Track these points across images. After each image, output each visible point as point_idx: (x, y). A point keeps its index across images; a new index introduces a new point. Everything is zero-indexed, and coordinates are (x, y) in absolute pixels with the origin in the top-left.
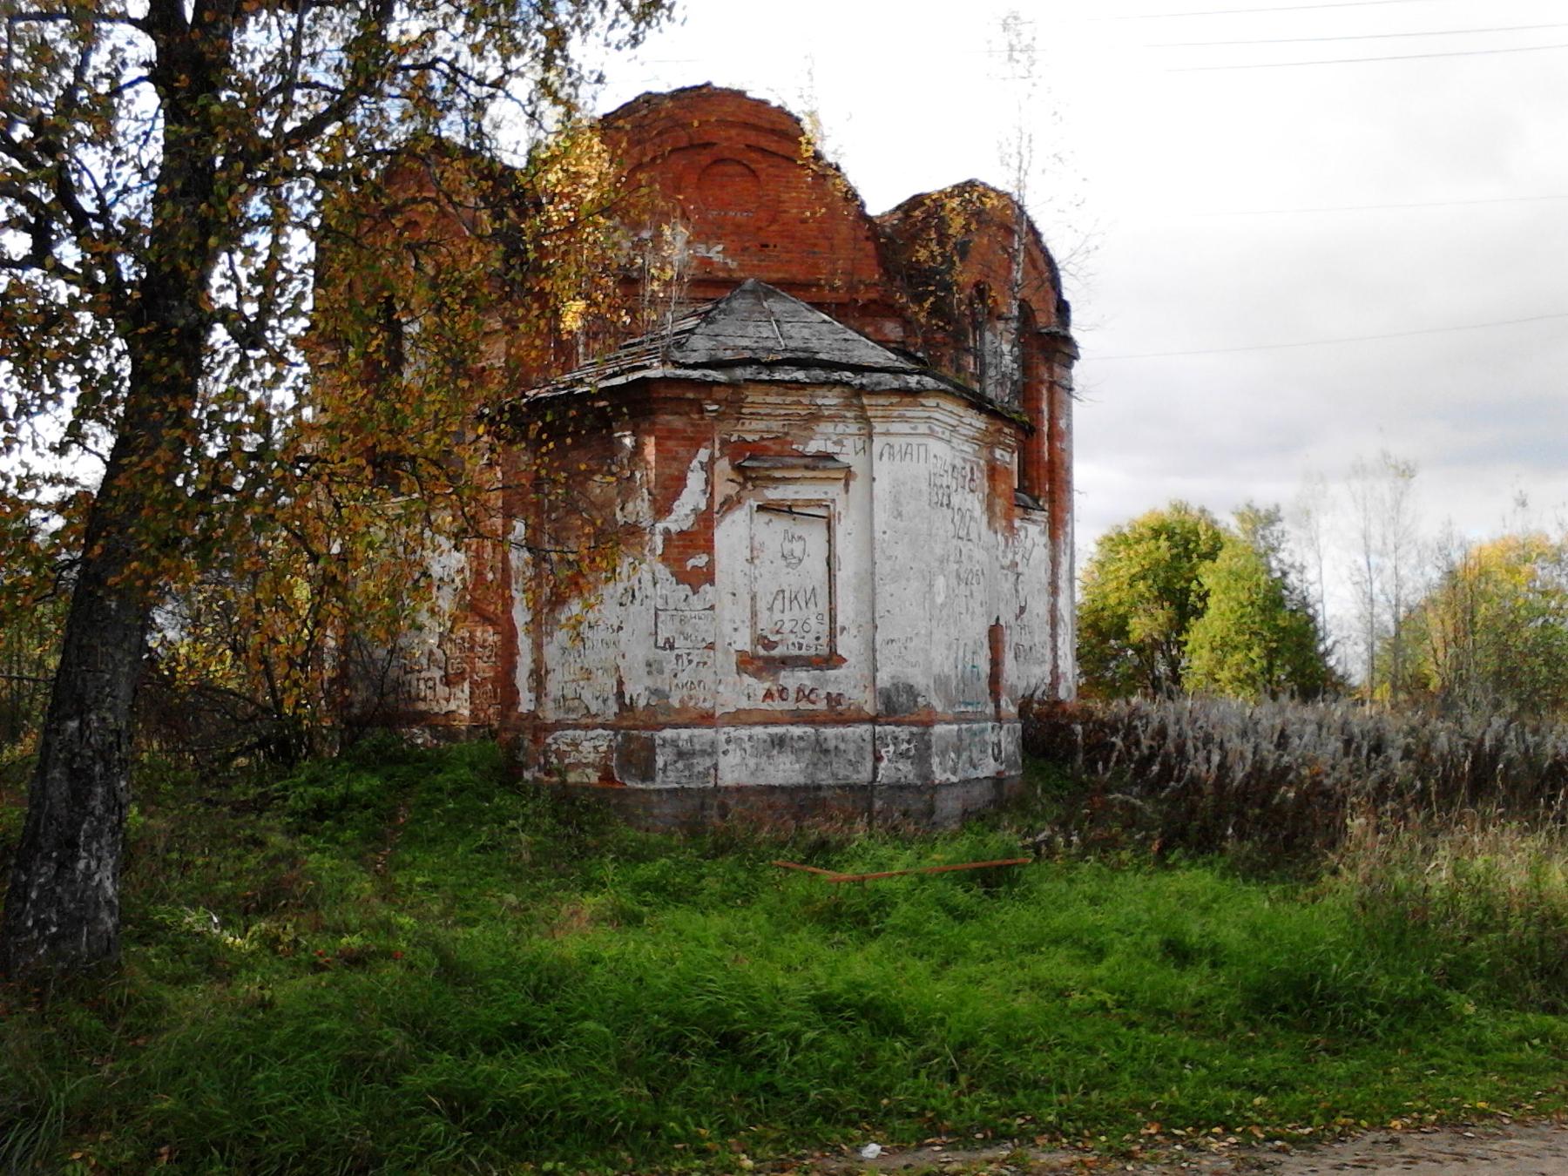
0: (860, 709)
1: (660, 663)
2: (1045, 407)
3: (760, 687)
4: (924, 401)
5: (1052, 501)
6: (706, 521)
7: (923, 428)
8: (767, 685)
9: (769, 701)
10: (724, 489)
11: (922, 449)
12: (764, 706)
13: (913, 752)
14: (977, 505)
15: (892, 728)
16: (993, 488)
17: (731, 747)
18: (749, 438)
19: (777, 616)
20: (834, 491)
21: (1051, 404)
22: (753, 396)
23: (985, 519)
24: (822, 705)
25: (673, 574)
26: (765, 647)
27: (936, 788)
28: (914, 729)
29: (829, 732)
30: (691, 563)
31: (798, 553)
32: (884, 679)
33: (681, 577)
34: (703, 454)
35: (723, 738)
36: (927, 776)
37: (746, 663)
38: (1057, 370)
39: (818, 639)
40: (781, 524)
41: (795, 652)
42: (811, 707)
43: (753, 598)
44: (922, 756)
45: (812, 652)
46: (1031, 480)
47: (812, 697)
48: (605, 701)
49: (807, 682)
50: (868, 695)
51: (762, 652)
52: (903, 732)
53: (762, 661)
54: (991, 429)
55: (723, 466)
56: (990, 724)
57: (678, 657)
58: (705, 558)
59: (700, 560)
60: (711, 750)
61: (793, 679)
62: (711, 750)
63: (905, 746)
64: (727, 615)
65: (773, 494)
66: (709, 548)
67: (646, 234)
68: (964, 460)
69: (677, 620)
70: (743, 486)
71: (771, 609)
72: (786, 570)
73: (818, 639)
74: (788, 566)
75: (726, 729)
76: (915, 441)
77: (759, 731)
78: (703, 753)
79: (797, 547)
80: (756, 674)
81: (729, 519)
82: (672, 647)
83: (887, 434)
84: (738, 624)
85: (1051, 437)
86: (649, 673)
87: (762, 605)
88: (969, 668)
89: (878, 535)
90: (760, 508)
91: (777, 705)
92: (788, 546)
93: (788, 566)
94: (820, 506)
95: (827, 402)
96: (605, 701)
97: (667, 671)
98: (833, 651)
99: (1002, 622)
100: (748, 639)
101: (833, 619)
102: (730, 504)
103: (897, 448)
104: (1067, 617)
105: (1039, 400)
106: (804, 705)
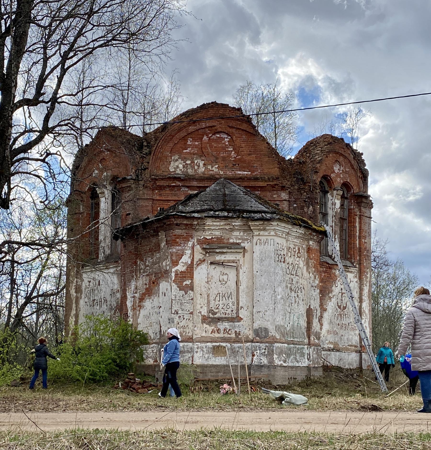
0: (248, 337)
1: (173, 319)
2: (357, 225)
3: (210, 328)
4: (272, 223)
5: (360, 264)
6: (191, 268)
7: (273, 233)
8: (213, 328)
9: (213, 334)
10: (198, 256)
11: (272, 240)
12: (211, 335)
13: (266, 353)
14: (301, 263)
15: (259, 344)
16: (309, 256)
17: (199, 350)
18: (208, 238)
19: (217, 303)
20: (239, 257)
21: (360, 223)
22: (209, 222)
23: (305, 268)
24: (233, 335)
25: (178, 287)
26: (212, 314)
27: (275, 367)
28: (267, 344)
29: (236, 345)
30: (185, 283)
31: (226, 280)
32: (256, 326)
33: (181, 288)
34: (190, 244)
35: (196, 346)
36: (271, 361)
37: (205, 320)
38: (363, 209)
39: (232, 311)
40: (219, 269)
41: (224, 316)
42: (229, 336)
43: (208, 296)
44: (270, 354)
45: (230, 316)
46: (351, 255)
47: (230, 332)
48: (156, 334)
49: (228, 327)
50: (251, 332)
51: (211, 316)
52: (263, 346)
53: (211, 319)
54: (307, 233)
55: (198, 248)
56: (306, 346)
57: (179, 317)
58: (190, 281)
59: (188, 282)
60: (191, 350)
61: (223, 326)
62: (191, 350)
63: (263, 351)
64: (198, 302)
65: (219, 258)
66: (192, 278)
67: (188, 162)
68: (295, 245)
69: (179, 304)
70: (205, 255)
71: (215, 300)
72: (221, 286)
73: (232, 311)
74: (221, 284)
75: (197, 343)
76: (269, 238)
77: (209, 344)
78: (188, 352)
79: (225, 277)
80: (209, 324)
81: (199, 267)
82: (177, 313)
83: (259, 235)
84: (202, 305)
85: (360, 237)
86: (169, 323)
87: (212, 298)
88: (296, 324)
89: (255, 272)
90: (212, 263)
91: (217, 335)
92: (221, 277)
93: (221, 284)
94: (234, 262)
95: (236, 224)
96: (156, 334)
97: (175, 322)
98: (238, 316)
99: (312, 307)
100: (206, 311)
101: (238, 304)
102: (202, 261)
103: (262, 241)
104: (367, 311)
105: (355, 222)
106: (226, 335)
